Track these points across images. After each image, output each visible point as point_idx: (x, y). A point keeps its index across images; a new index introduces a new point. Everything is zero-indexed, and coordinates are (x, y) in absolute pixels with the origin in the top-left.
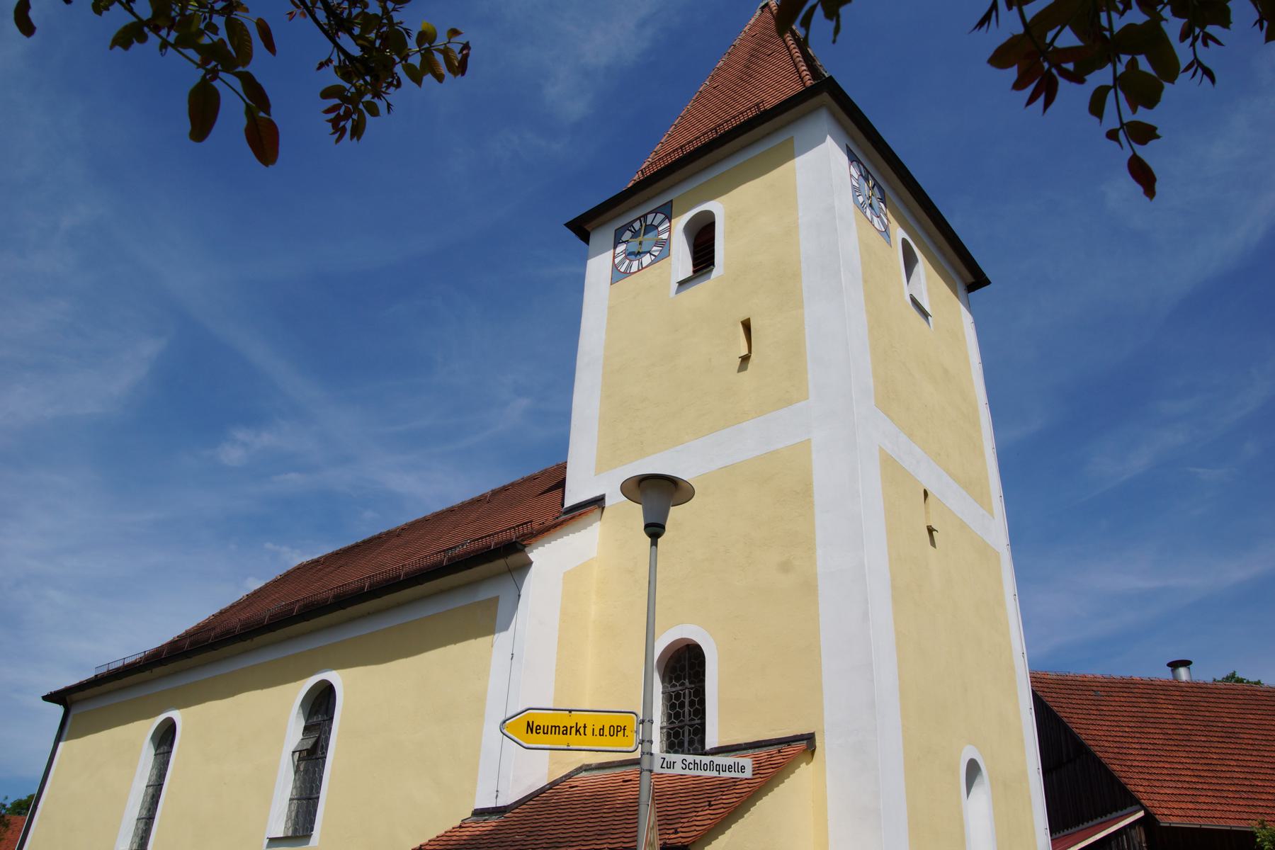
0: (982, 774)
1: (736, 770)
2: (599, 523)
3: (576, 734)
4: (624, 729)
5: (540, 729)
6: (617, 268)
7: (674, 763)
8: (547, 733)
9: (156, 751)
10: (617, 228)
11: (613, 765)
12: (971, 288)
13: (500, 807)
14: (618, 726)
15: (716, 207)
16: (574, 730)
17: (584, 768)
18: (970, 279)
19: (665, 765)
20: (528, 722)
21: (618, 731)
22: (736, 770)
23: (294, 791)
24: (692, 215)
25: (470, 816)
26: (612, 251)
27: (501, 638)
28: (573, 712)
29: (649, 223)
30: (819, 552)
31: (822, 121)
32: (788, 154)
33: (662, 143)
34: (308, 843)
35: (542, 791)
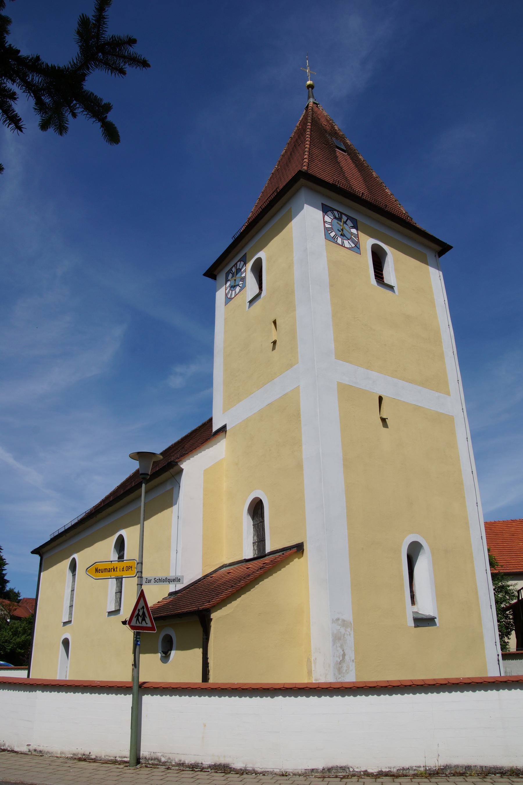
0: (423, 549)
1: (177, 581)
2: (225, 439)
3: (113, 571)
4: (132, 567)
5: (100, 571)
6: (227, 296)
7: (151, 580)
8: (103, 572)
9: (73, 574)
10: (226, 272)
11: (234, 563)
12: (441, 254)
13: (177, 591)
14: (129, 566)
15: (261, 254)
16: (113, 570)
17: (224, 566)
18: (439, 248)
19: (147, 582)
20: (96, 568)
21: (129, 569)
22: (177, 581)
23: (117, 588)
24: (254, 261)
25: (167, 596)
26: (225, 285)
27: (175, 508)
28: (112, 562)
29: (238, 268)
30: (304, 447)
31: (303, 194)
32: (289, 219)
33: (252, 212)
34: (119, 614)
35: (199, 580)
